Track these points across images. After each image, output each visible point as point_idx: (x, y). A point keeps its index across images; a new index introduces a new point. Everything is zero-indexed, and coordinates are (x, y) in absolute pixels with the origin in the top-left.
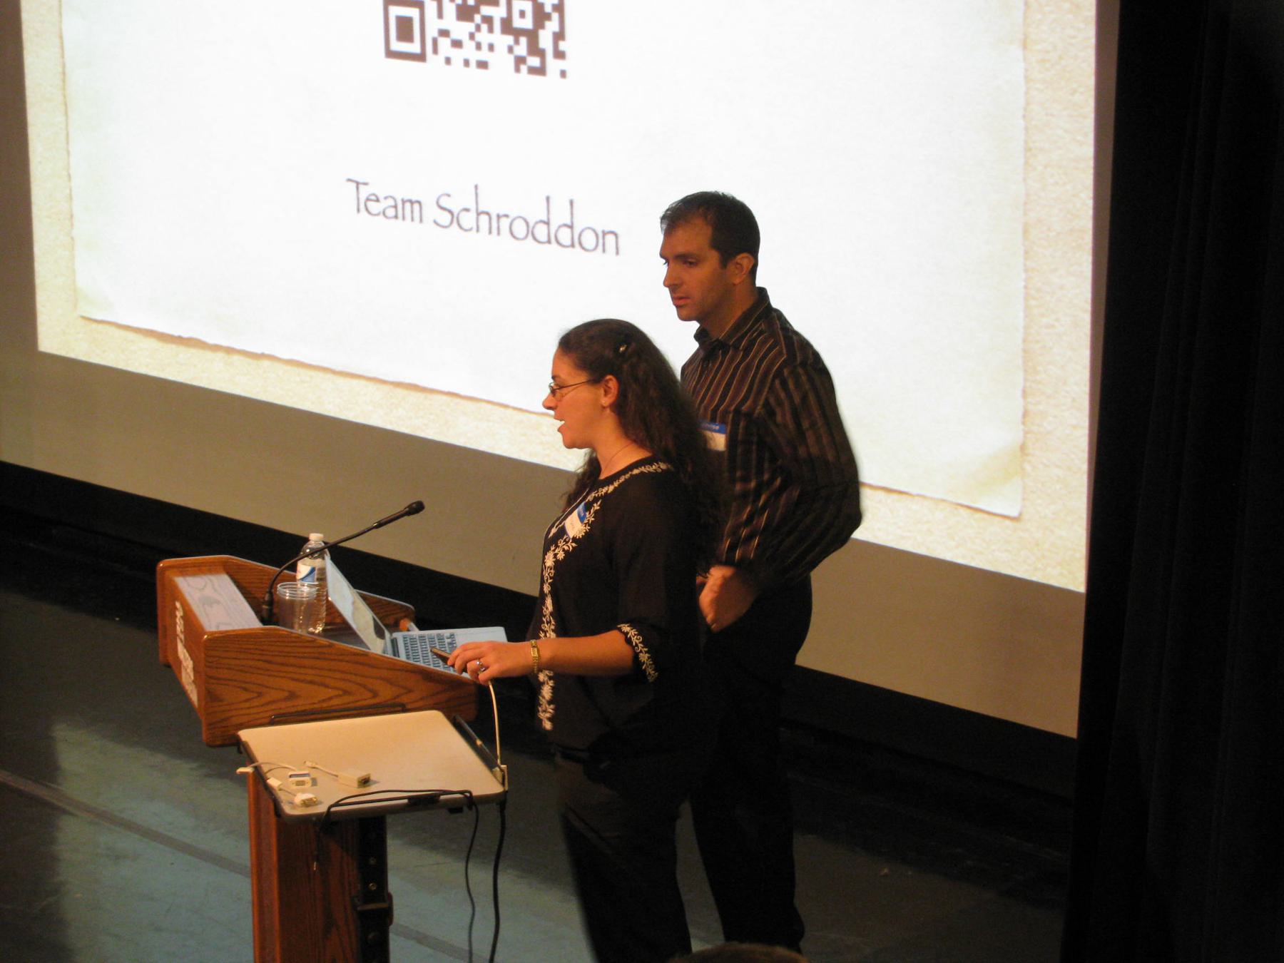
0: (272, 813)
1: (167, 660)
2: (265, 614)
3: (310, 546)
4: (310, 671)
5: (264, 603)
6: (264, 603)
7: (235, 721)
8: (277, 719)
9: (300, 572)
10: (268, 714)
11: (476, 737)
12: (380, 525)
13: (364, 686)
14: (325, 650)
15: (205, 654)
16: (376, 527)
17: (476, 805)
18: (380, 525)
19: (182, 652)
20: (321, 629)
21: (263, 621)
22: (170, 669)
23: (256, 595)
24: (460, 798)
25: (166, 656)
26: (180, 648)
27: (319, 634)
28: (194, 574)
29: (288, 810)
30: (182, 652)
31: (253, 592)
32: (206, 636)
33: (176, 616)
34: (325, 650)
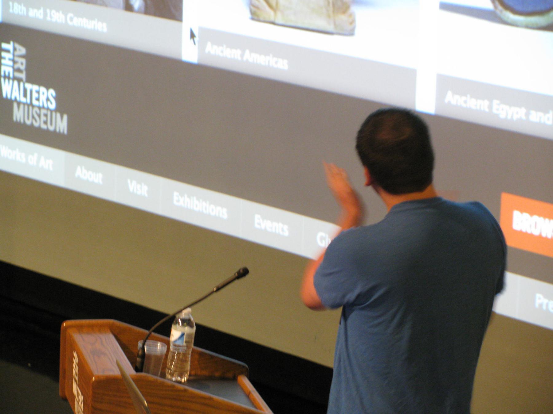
2: (138, 365)
3: (181, 317)
5: (138, 356)
9: (173, 336)
12: (218, 289)
18: (218, 289)
21: (137, 370)
24: (145, 405)
26: (75, 386)
27: (184, 384)
33: (73, 362)
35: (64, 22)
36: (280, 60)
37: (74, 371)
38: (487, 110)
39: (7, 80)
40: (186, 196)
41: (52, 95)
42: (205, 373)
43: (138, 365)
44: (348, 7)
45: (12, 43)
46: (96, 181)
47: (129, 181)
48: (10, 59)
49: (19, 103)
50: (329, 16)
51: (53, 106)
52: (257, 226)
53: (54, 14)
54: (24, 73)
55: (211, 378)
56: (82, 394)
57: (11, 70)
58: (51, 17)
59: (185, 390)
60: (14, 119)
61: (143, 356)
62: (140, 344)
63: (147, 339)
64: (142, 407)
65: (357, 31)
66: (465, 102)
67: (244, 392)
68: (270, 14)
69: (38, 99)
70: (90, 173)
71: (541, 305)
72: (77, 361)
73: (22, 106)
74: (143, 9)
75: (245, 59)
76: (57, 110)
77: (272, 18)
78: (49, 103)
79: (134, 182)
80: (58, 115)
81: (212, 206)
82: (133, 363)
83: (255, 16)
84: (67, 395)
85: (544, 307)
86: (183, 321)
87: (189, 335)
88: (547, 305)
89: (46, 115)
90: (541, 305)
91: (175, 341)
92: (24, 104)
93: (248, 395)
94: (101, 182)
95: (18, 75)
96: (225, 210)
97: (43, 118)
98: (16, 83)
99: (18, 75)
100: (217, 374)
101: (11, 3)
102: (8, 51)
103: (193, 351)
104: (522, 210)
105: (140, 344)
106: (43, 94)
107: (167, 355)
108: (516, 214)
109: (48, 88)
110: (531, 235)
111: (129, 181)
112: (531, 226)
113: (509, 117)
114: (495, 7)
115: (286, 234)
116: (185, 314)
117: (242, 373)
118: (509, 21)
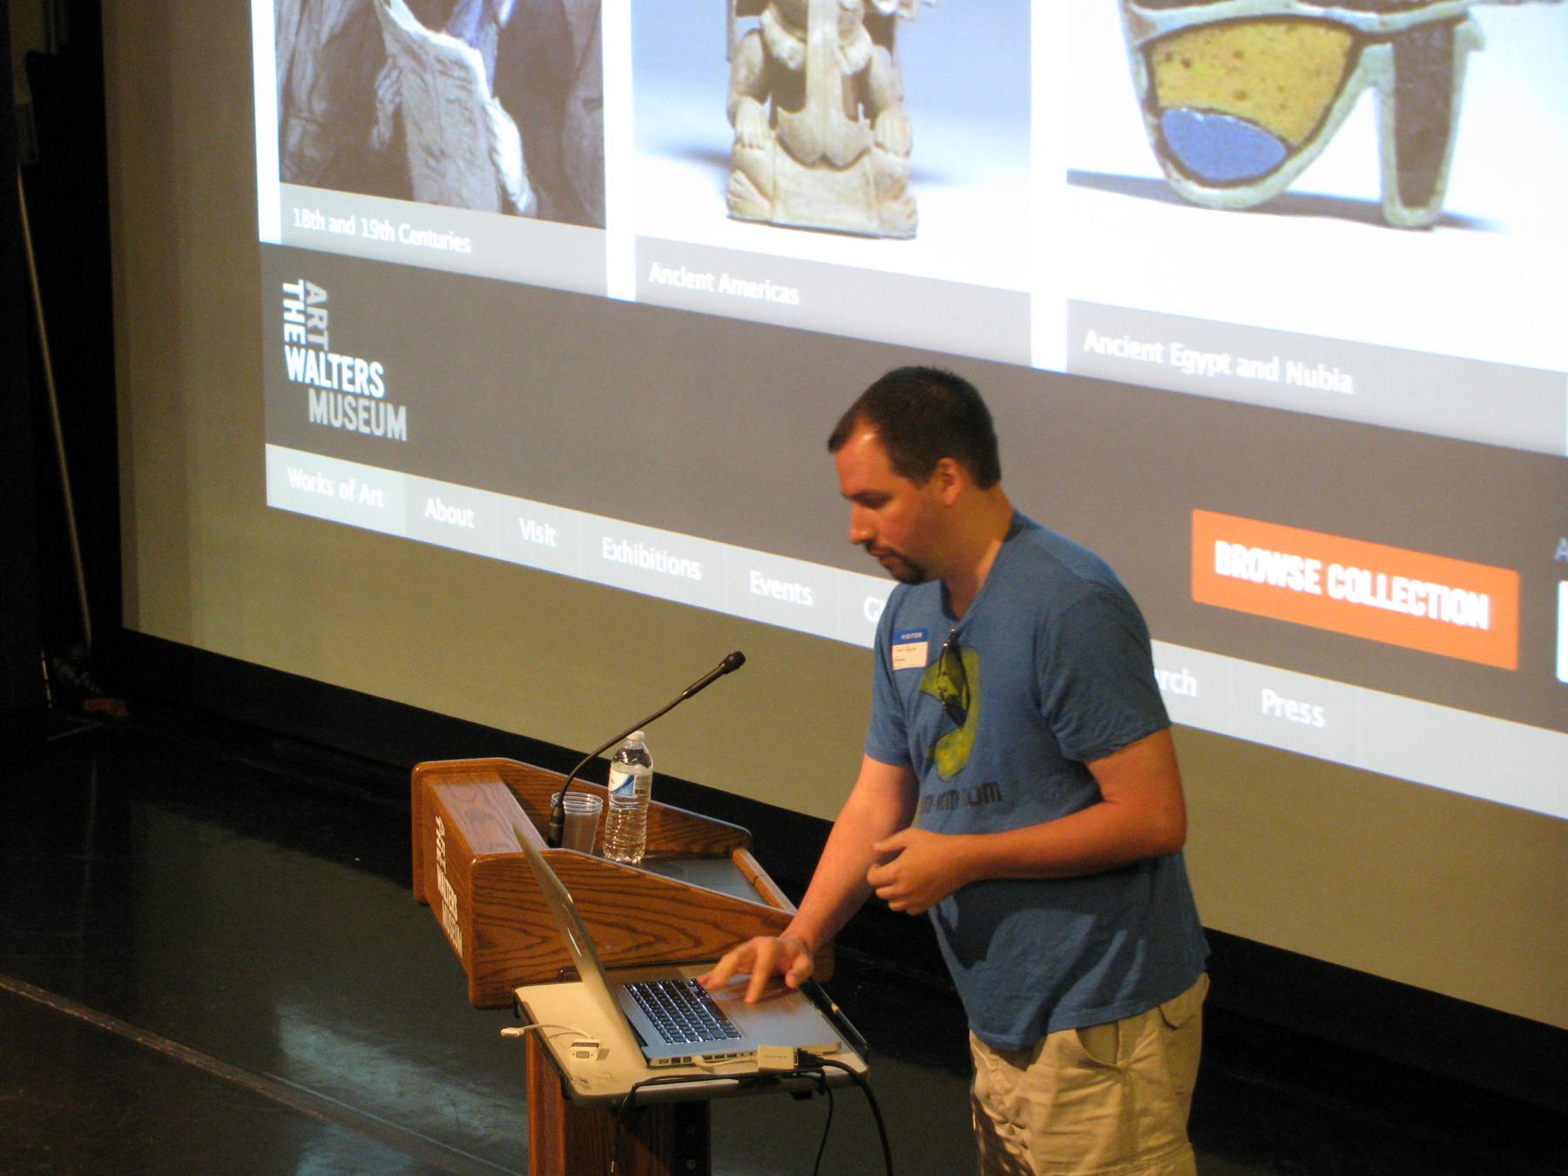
0: (559, 1091)
1: (423, 896)
2: (553, 835)
3: (626, 747)
4: (610, 910)
6: (552, 819)
7: (512, 974)
8: (566, 974)
10: (554, 966)
11: (831, 1001)
12: (691, 693)
13: (683, 931)
14: (632, 882)
15: (473, 884)
16: (687, 696)
17: (829, 1090)
19: (443, 884)
20: (639, 858)
21: (551, 843)
22: (428, 908)
23: (541, 812)
25: (422, 891)
27: (636, 865)
28: (459, 783)
29: (580, 1089)
30: (443, 884)
31: (538, 807)
32: (474, 861)
33: (436, 836)
34: (632, 882)
35: (393, 239)
36: (784, 289)
37: (438, 851)
38: (1161, 361)
39: (295, 349)
40: (625, 542)
41: (377, 372)
42: (674, 846)
43: (553, 835)
44: (903, 188)
45: (301, 282)
46: (463, 523)
47: (521, 520)
48: (299, 312)
49: (319, 389)
50: (869, 206)
51: (379, 392)
52: (754, 590)
53: (375, 226)
54: (326, 333)
55: (685, 856)
56: (455, 892)
57: (302, 330)
58: (370, 232)
59: (639, 876)
60: (312, 419)
61: (561, 819)
62: (554, 798)
63: (565, 790)
64: (564, 906)
65: (919, 231)
66: (1121, 348)
67: (747, 878)
68: (763, 208)
69: (352, 381)
70: (451, 509)
71: (1272, 709)
72: (443, 834)
73: (324, 394)
74: (534, 208)
75: (720, 290)
76: (385, 399)
77: (767, 216)
78: (372, 386)
79: (531, 523)
80: (390, 407)
81: (673, 559)
82: (544, 832)
83: (736, 212)
84: (429, 896)
85: (1278, 713)
86: (631, 754)
87: (643, 779)
88: (1283, 707)
89: (367, 409)
90: (1272, 709)
91: (617, 791)
92: (328, 390)
93: (753, 883)
94: (471, 525)
95: (314, 339)
96: (696, 565)
97: (363, 415)
98: (311, 353)
99: (314, 339)
100: (696, 848)
101: (296, 211)
102: (295, 297)
103: (651, 808)
104: (1231, 539)
105: (554, 798)
106: (362, 370)
107: (603, 817)
108: (1221, 546)
109: (369, 360)
110: (1249, 583)
111: (521, 520)
112: (1248, 568)
113: (1201, 372)
114: (1168, 174)
115: (809, 602)
116: (634, 740)
117: (740, 845)
118: (1193, 198)
